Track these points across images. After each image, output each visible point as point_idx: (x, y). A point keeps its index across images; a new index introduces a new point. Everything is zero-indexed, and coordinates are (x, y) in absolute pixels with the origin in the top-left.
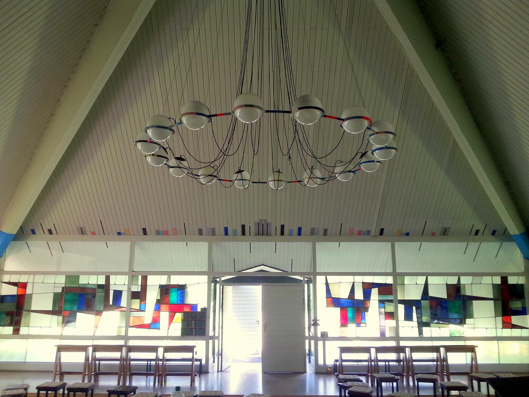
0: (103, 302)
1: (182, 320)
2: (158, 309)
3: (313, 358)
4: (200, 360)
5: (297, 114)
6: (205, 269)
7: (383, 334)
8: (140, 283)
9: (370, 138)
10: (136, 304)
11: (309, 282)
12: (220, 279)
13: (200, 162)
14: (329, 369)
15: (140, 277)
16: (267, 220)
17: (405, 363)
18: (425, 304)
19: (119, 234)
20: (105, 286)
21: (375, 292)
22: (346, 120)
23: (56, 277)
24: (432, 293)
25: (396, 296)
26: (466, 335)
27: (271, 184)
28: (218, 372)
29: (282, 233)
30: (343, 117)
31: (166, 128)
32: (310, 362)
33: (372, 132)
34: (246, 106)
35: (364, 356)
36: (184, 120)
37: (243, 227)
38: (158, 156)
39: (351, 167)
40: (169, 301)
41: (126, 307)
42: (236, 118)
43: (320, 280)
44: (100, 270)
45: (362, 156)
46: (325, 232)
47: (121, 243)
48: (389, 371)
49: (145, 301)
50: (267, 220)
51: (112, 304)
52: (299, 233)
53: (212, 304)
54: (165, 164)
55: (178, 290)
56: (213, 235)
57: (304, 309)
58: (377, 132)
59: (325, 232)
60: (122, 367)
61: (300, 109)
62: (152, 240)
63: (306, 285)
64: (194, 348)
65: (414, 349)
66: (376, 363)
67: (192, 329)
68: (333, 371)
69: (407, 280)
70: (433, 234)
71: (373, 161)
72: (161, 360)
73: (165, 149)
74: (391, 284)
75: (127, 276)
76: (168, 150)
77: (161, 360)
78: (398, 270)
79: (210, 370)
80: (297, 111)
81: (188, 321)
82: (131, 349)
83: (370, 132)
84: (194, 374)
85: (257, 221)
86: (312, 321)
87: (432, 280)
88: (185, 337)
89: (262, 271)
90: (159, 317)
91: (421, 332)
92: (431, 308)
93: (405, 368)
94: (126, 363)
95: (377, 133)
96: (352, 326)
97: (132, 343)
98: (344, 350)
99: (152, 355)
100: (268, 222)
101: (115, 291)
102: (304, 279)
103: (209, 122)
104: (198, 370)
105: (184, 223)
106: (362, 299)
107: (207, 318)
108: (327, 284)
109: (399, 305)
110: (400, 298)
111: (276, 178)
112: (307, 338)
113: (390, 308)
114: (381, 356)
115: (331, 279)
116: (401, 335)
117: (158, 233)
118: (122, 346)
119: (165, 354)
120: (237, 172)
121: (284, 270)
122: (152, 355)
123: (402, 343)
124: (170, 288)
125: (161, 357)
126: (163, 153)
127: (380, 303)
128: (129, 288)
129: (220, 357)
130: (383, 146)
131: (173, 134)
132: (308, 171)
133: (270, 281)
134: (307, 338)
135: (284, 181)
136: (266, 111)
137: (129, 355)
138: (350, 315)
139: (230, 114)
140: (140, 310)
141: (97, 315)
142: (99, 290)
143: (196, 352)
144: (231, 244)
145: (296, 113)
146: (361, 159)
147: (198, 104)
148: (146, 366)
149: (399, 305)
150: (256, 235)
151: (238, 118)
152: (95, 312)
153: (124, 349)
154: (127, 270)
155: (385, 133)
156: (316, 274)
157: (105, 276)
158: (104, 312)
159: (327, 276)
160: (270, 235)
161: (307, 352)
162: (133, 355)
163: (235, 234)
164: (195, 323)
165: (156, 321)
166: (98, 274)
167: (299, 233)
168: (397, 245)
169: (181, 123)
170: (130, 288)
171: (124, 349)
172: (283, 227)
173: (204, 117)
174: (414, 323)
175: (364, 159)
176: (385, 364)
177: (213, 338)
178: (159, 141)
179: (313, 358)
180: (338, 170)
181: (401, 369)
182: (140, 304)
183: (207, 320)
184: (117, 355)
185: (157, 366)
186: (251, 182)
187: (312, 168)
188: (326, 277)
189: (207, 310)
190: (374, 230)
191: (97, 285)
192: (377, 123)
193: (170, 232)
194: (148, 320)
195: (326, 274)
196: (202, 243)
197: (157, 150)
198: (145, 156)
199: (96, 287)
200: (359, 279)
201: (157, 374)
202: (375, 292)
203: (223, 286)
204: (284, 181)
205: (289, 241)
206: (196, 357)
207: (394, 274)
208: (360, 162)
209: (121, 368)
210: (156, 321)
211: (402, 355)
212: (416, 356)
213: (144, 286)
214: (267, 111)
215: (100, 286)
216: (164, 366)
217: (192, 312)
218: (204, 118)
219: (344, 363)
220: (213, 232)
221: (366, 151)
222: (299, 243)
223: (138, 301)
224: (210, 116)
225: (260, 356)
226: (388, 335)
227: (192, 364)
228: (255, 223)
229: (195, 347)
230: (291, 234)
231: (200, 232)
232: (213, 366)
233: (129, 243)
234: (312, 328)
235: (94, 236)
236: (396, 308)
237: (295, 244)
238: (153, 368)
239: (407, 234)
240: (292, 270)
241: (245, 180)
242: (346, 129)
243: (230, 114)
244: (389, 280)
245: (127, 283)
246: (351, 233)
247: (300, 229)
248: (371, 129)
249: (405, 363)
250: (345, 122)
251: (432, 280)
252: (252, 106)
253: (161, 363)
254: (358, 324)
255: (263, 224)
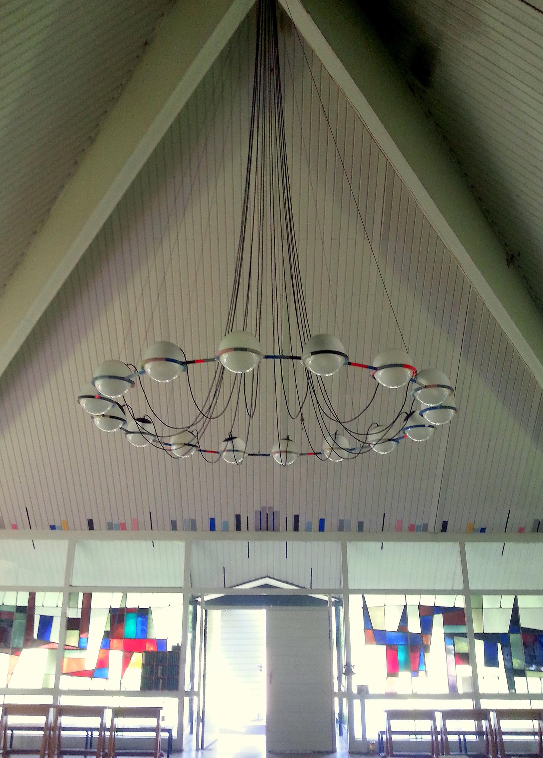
0: (23, 634)
1: (143, 665)
2: (106, 646)
3: (346, 727)
4: (169, 731)
5: (310, 361)
6: (180, 583)
7: (453, 688)
8: (80, 605)
9: (416, 393)
10: (73, 637)
11: (337, 604)
12: (203, 599)
13: (169, 427)
14: (371, 746)
15: (81, 595)
16: (273, 508)
17: (489, 737)
18: (515, 638)
19: (53, 528)
20: (27, 609)
21: (438, 619)
22: (380, 369)
23: (5, 595)
24: (524, 623)
25: (471, 628)
26: (400, 691)
27: (276, 457)
28: (197, 749)
29: (296, 528)
30: (375, 365)
31: (122, 379)
32: (341, 734)
33: (418, 386)
34: (236, 349)
35: (425, 725)
36: (148, 368)
37: (238, 517)
38: (111, 417)
39: (392, 433)
40: (123, 633)
41: (58, 642)
42: (220, 366)
43: (355, 601)
44: (21, 583)
45: (406, 419)
46: (360, 527)
47: (55, 542)
48: (466, 751)
49: (87, 633)
50: (272, 508)
51: (36, 638)
52: (322, 528)
53: (190, 636)
54: (121, 428)
55: (138, 617)
56: (320, 531)
57: (331, 649)
58: (426, 386)
59: (360, 527)
60: (48, 739)
61: (313, 353)
62: (101, 539)
63: (333, 609)
64: (161, 711)
65: (502, 714)
66: (444, 737)
67: (158, 679)
68: (377, 750)
69: (487, 602)
70: (521, 530)
71: (424, 426)
72: (108, 730)
73: (121, 408)
74: (463, 608)
75: (62, 594)
76: (125, 408)
77: (108, 730)
78: (473, 586)
79: (185, 747)
80: (309, 357)
81: (152, 666)
82: (62, 711)
83: (415, 386)
84: (158, 754)
85: (258, 509)
86: (344, 668)
87: (524, 602)
88: (147, 692)
89: (267, 586)
90: (107, 658)
91: (511, 685)
92: (525, 645)
93: (491, 748)
94: (54, 734)
95: (426, 387)
96: (404, 675)
97: (65, 701)
98: (393, 715)
99: (94, 722)
100: (275, 510)
101: (43, 618)
102: (330, 599)
103: (184, 371)
104: (166, 747)
105: (384, 514)
106: (420, 632)
107: (181, 662)
108: (365, 608)
109: (475, 640)
110: (477, 629)
111: (283, 449)
112: (336, 695)
113: (463, 646)
114: (453, 725)
115: (371, 600)
116: (482, 691)
117: (110, 526)
118: (50, 706)
119: (116, 719)
120: (227, 440)
121: (300, 585)
122: (94, 722)
123: (485, 704)
124: (125, 613)
125: (108, 726)
126: (120, 414)
127: (446, 638)
128: (64, 613)
129: (201, 724)
130: (435, 405)
131: (132, 387)
132: (329, 439)
133: (278, 603)
134: (336, 695)
135: (294, 453)
136: (265, 356)
137: (59, 721)
138: (401, 656)
139: (212, 360)
140: (81, 648)
141: (13, 654)
142: (17, 615)
143: (163, 718)
144: (220, 543)
145: (308, 359)
146: (405, 422)
147: (168, 345)
148: (85, 739)
149: (476, 641)
150: (257, 530)
151: (226, 366)
152: (10, 650)
153: (52, 710)
154: (62, 584)
155: (438, 387)
156: (348, 592)
157: (28, 593)
158: (24, 649)
159: (365, 595)
160: (279, 531)
161: (337, 716)
162: (66, 721)
163: (226, 528)
164: (162, 670)
165: (102, 664)
166: (17, 589)
167: (322, 528)
168: (469, 547)
169: (143, 372)
170: (66, 613)
171: (52, 711)
172: (296, 518)
173: (176, 364)
174: (501, 670)
175: (410, 423)
176: (534, 739)
177: (191, 694)
178: (112, 397)
179: (346, 727)
180: (372, 438)
181: (483, 748)
182: (80, 637)
183: (181, 666)
184: (40, 720)
185: (102, 738)
186: (246, 455)
187: (336, 434)
188: (363, 597)
189: (181, 649)
190: (434, 524)
191: (16, 607)
192: (425, 373)
193: (129, 525)
194: (90, 664)
195: (363, 592)
196: (176, 542)
197: (109, 408)
198: (92, 417)
199: (14, 610)
200: (414, 601)
201: (102, 753)
202: (438, 619)
203: (206, 611)
204: (294, 453)
205: (305, 540)
206: (163, 725)
207: (466, 592)
208: (405, 427)
209: (46, 744)
210: (102, 664)
211: (484, 723)
212: (507, 725)
213: (87, 610)
214: (267, 357)
215: (20, 609)
216: (113, 739)
217: (157, 652)
218: (177, 365)
219: (395, 737)
220: (193, 526)
221: (411, 411)
222: (321, 544)
223: (77, 632)
224: (185, 364)
225: (264, 723)
226: (461, 690)
227: (157, 736)
228: (256, 512)
229: (161, 708)
230: (309, 529)
231: (174, 526)
232: (190, 741)
233: (66, 542)
234: (344, 677)
235: (54, 531)
236: (472, 646)
237: (315, 544)
238: (95, 743)
239: (483, 530)
240: (311, 586)
241: (238, 451)
242: (381, 381)
243: (212, 360)
244: (459, 602)
245: (60, 605)
246: (399, 528)
247: (322, 522)
248: (416, 382)
249: (489, 737)
250: (378, 372)
251: (524, 602)
252: (245, 349)
253: (108, 734)
254: (415, 671)
255: (267, 514)
